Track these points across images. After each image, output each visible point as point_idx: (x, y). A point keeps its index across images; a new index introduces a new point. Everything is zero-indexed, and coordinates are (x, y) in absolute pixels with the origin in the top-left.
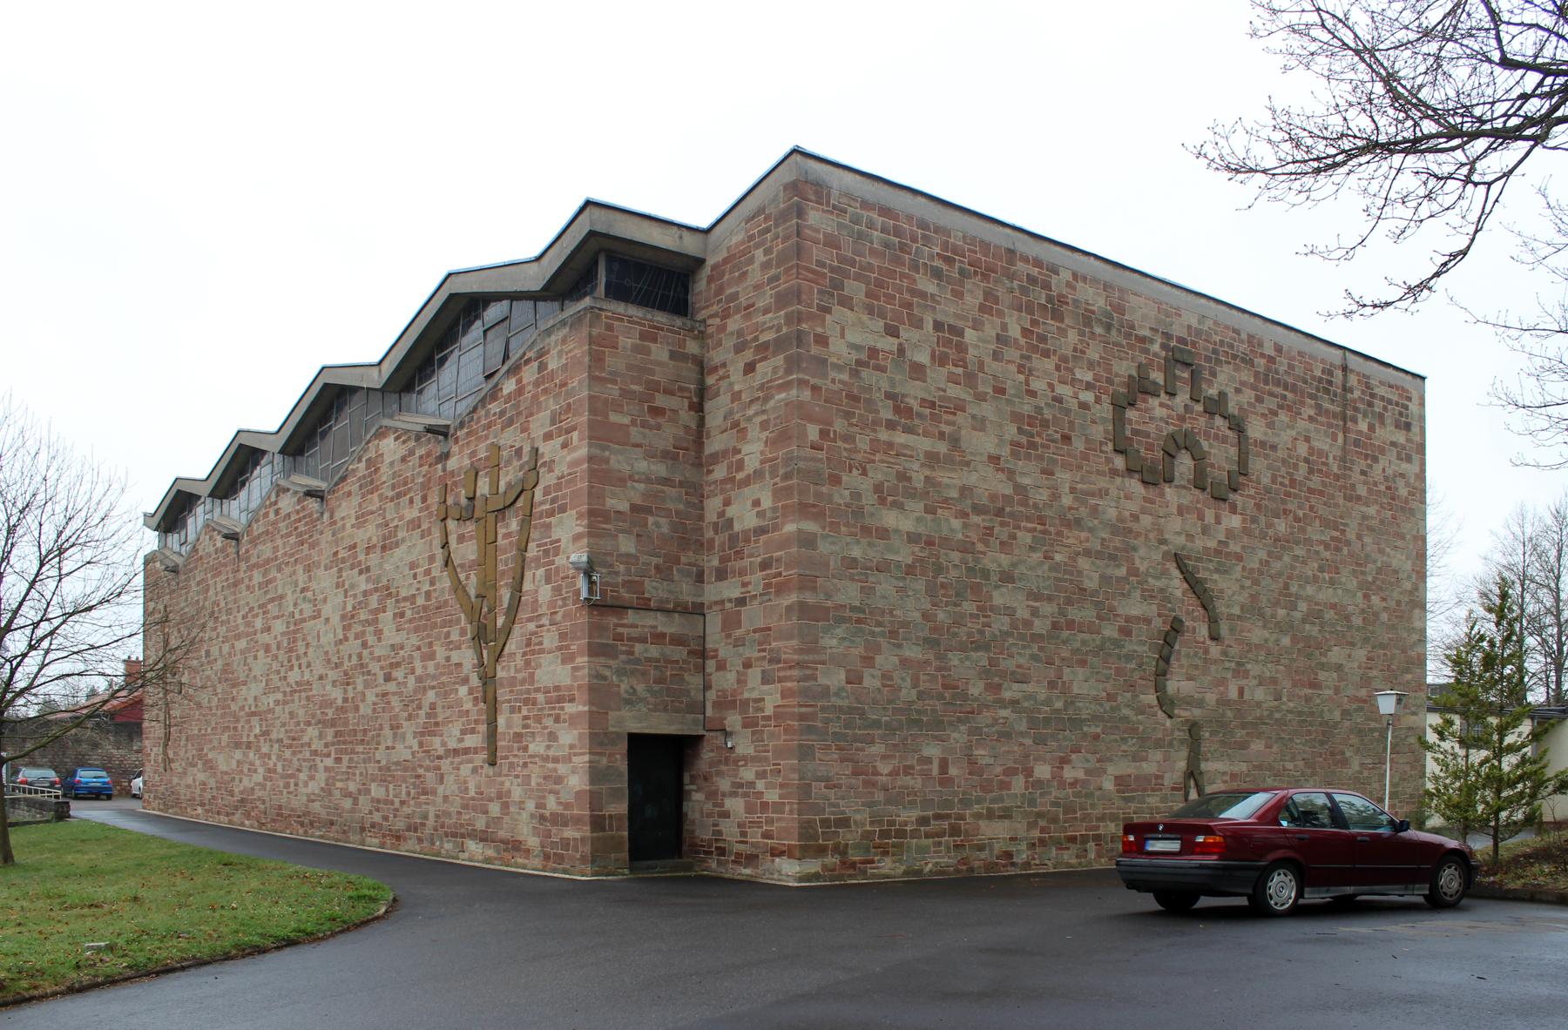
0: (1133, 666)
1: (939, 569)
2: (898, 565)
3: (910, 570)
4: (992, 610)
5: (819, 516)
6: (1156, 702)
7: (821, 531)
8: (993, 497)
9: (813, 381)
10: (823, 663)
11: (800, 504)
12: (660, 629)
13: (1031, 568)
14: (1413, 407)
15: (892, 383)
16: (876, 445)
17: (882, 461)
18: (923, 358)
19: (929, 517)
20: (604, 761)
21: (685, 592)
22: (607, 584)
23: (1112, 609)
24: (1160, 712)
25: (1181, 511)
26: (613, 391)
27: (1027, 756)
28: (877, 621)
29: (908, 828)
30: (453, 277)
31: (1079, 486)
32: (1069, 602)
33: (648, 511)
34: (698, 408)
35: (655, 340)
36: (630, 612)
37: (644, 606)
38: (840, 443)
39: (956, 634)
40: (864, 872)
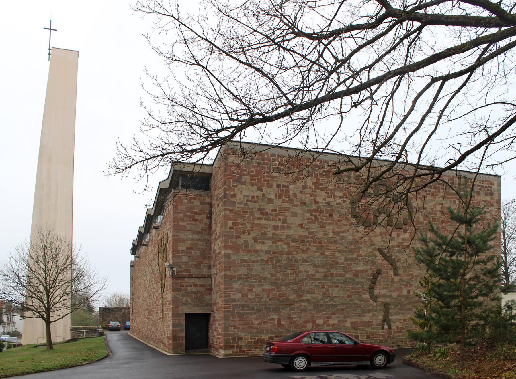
0: (359, 286)
1: (278, 261)
2: (262, 261)
3: (266, 262)
4: (299, 272)
5: (232, 248)
6: (369, 297)
7: (233, 253)
8: (300, 237)
9: (230, 208)
10: (233, 292)
11: (225, 245)
12: (196, 283)
13: (315, 258)
14: (494, 187)
15: (260, 205)
16: (253, 225)
17: (256, 230)
18: (272, 196)
19: (274, 245)
20: (177, 321)
21: (205, 272)
22: (179, 271)
23: (350, 268)
24: (371, 301)
25: (381, 234)
26: (181, 216)
27: (313, 317)
28: (253, 278)
29: (265, 340)
30: (160, 184)
31: (336, 230)
32: (331, 267)
33: (192, 249)
34: (210, 217)
35: (195, 199)
36: (186, 278)
37: (191, 276)
38: (240, 226)
39: (284, 281)
40: (248, 354)
